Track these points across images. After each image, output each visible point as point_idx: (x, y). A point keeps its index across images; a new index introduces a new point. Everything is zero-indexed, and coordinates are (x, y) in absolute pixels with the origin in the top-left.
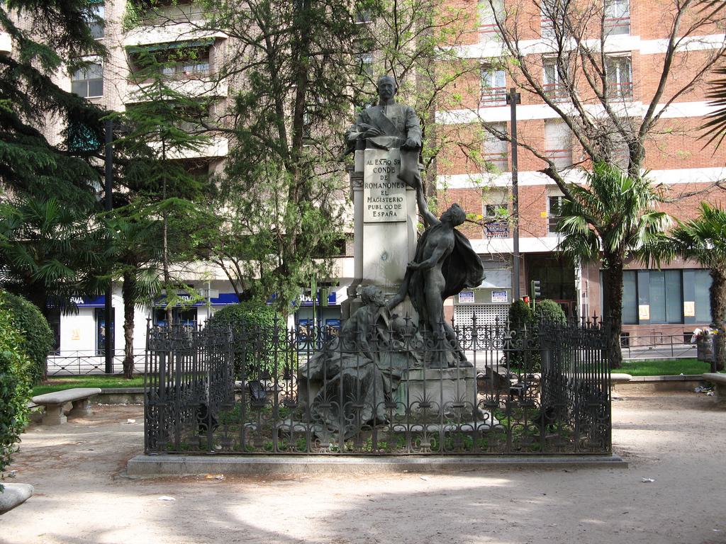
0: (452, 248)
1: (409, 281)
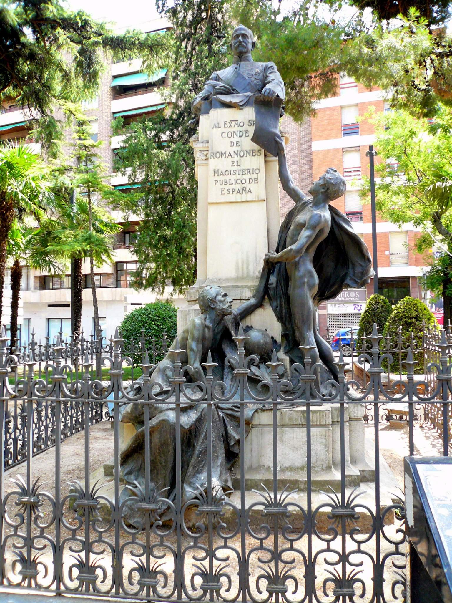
0: (327, 231)
1: (268, 279)
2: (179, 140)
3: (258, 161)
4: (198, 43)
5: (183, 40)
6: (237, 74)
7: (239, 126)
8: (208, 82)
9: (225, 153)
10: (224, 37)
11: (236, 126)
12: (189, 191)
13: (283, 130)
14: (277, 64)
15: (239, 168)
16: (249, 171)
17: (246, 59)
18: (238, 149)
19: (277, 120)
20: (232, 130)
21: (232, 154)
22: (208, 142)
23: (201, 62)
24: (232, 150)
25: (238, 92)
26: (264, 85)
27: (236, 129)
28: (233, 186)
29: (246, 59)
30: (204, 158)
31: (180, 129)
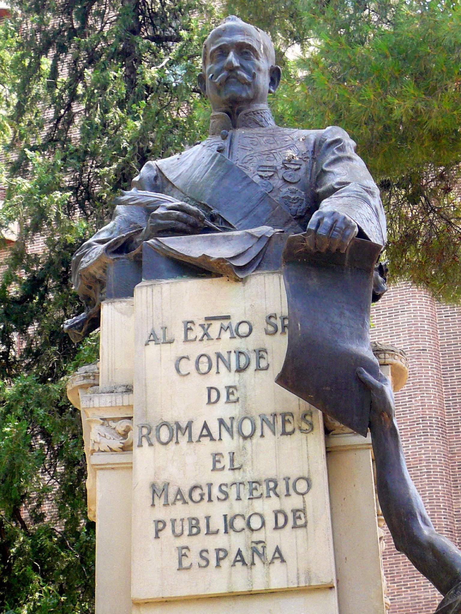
2: (28, 368)
3: (304, 453)
4: (92, 61)
5: (44, 51)
6: (224, 167)
7: (236, 334)
8: (130, 194)
9: (189, 425)
10: (179, 39)
11: (226, 335)
12: (62, 544)
13: (383, 342)
14: (351, 127)
15: (238, 476)
16: (272, 486)
17: (255, 122)
18: (234, 410)
19: (362, 312)
20: (210, 349)
21: (214, 427)
22: (129, 390)
23: (102, 118)
24: (212, 415)
25: (227, 226)
26: (315, 202)
27: (226, 344)
28: (221, 541)
29: (255, 122)
30: (117, 444)
31: (31, 330)
